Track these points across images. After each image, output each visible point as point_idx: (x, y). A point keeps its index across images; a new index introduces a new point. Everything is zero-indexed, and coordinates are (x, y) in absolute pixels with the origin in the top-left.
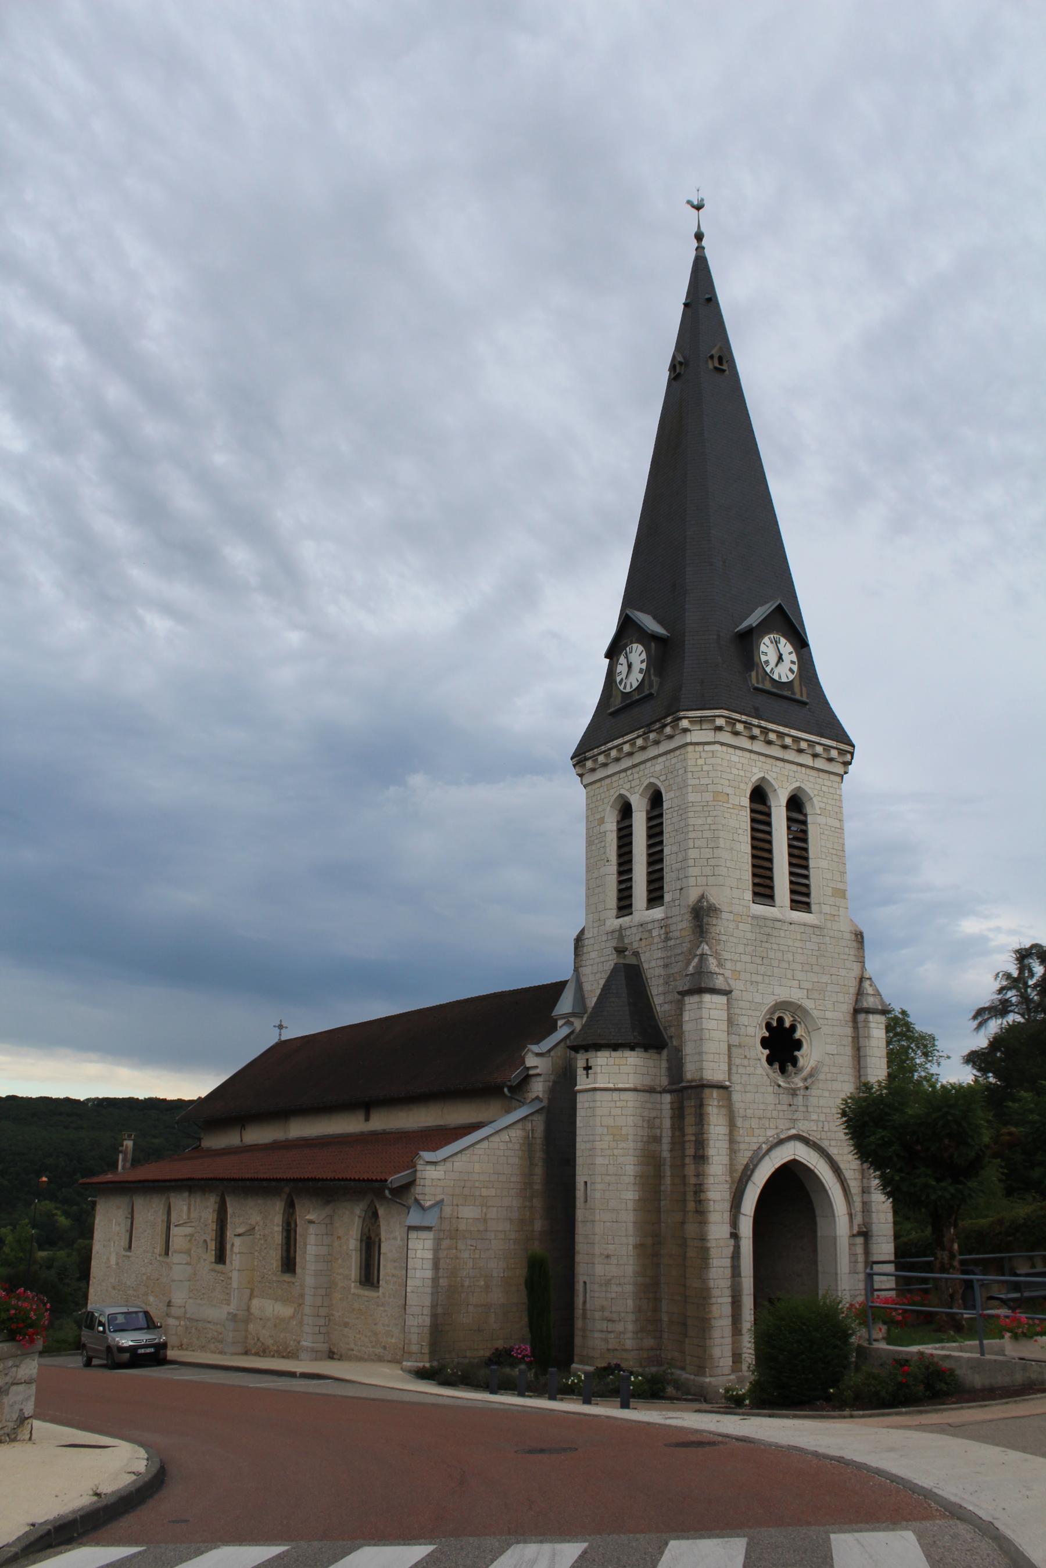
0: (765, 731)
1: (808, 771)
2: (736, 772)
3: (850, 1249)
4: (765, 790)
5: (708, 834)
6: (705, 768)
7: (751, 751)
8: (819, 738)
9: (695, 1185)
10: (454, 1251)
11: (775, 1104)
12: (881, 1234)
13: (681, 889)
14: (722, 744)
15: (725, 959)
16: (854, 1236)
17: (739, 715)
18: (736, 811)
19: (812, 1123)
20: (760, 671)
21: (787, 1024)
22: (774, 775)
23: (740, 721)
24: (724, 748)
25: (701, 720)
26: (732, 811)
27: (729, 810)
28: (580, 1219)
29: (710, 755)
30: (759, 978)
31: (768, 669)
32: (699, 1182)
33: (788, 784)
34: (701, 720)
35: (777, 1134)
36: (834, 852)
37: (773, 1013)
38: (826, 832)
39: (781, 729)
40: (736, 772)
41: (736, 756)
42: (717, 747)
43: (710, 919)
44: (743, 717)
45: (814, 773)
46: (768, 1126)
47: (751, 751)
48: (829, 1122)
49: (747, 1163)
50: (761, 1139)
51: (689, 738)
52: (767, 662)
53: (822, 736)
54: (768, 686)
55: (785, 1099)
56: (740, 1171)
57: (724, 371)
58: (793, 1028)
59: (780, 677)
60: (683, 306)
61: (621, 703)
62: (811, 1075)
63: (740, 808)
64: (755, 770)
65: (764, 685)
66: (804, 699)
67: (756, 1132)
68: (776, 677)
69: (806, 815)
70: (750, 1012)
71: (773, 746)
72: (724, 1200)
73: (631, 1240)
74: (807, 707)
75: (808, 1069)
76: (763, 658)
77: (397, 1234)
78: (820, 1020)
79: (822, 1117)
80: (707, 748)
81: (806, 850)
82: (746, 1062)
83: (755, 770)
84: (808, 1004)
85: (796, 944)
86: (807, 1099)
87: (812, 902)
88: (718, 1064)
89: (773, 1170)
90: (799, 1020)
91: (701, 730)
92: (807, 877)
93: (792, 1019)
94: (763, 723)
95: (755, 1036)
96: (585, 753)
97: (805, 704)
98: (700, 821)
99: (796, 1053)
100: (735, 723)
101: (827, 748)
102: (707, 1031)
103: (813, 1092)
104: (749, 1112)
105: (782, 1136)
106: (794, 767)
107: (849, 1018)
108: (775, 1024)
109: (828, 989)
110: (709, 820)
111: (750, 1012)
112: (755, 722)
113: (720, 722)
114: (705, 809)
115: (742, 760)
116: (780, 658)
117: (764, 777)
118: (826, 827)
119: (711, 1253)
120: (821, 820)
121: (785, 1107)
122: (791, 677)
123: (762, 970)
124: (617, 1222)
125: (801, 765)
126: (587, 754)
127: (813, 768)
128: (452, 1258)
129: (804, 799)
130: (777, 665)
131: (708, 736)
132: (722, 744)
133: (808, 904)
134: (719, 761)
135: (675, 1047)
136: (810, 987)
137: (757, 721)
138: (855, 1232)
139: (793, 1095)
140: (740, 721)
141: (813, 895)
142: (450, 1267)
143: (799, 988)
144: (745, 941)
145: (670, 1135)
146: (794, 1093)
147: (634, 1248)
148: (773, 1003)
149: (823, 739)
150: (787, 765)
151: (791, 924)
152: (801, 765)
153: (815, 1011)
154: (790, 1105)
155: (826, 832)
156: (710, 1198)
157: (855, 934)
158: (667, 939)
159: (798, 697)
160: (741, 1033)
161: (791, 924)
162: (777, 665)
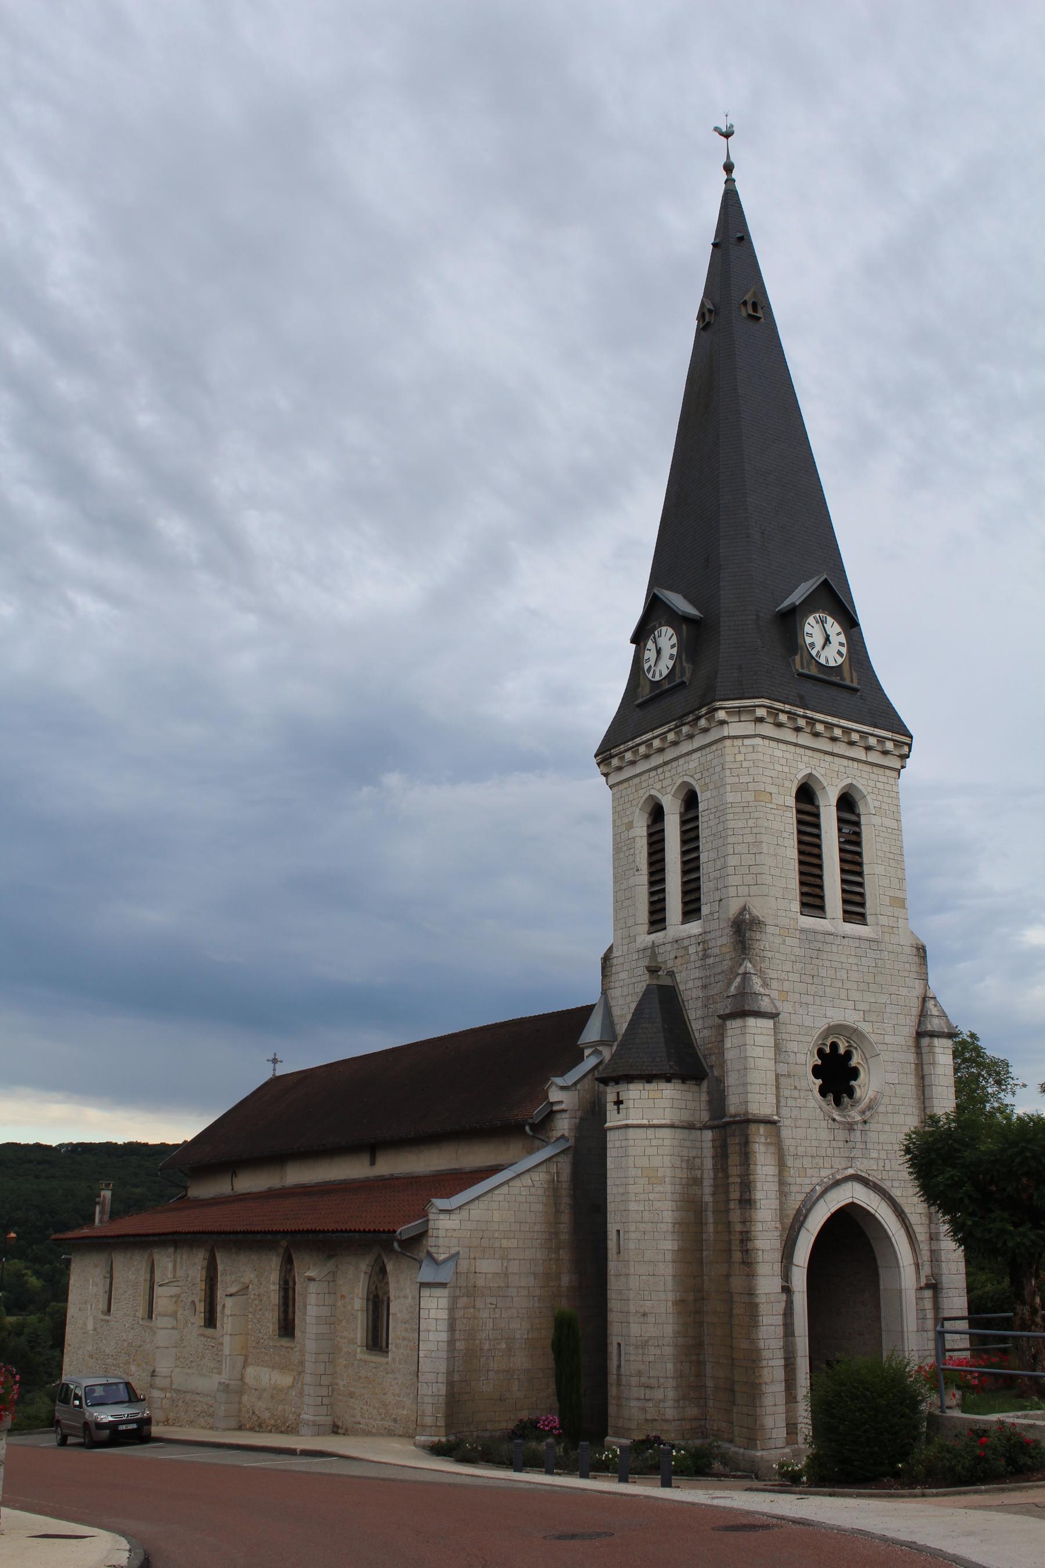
0: (811, 722)
3: (917, 1304)
5: (750, 839)
6: (745, 764)
7: (796, 745)
8: (873, 729)
9: (742, 1232)
10: (472, 1310)
11: (830, 1141)
12: (952, 1286)
13: (720, 900)
14: (764, 737)
15: (770, 978)
16: (921, 1288)
19: (872, 1161)
21: (842, 1050)
22: (823, 771)
23: (783, 711)
24: (766, 742)
25: (739, 711)
29: (751, 749)
30: (809, 999)
32: (745, 1230)
34: (739, 711)
35: (832, 1174)
36: (892, 856)
37: (826, 1038)
38: (882, 834)
39: (830, 719)
41: (779, 751)
43: (753, 934)
44: (786, 706)
46: (822, 1165)
47: (796, 745)
48: (890, 1160)
49: (800, 1207)
50: (815, 1180)
52: (812, 645)
54: (814, 671)
55: (842, 1134)
56: (792, 1217)
57: (759, 318)
58: (848, 1054)
59: (827, 661)
61: (650, 693)
62: (870, 1108)
63: (785, 809)
64: (801, 766)
65: (809, 670)
66: (855, 685)
67: (809, 1172)
69: (859, 815)
70: (800, 1038)
72: (774, 1249)
73: (671, 1296)
75: (867, 1100)
78: (878, 1045)
79: (883, 1155)
80: (747, 742)
81: (860, 854)
82: (796, 1094)
83: (801, 766)
84: (865, 1028)
85: (850, 961)
86: (866, 1134)
87: (868, 913)
88: (765, 1095)
89: (829, 1214)
90: (855, 1045)
91: (740, 721)
92: (861, 885)
93: (847, 1044)
94: (809, 713)
95: (806, 1064)
96: (610, 750)
97: (856, 690)
98: (740, 824)
99: (853, 1083)
100: (778, 714)
102: (752, 1059)
103: (873, 1126)
104: (801, 1150)
105: (838, 1177)
106: (845, 762)
107: (911, 1042)
108: (828, 1050)
109: (888, 1010)
110: (751, 823)
111: (800, 1038)
112: (800, 711)
113: (761, 712)
114: (746, 810)
115: (787, 755)
118: (881, 829)
119: (760, 1309)
120: (876, 820)
121: (841, 1144)
123: (812, 989)
124: (654, 1275)
125: (853, 759)
127: (866, 762)
128: (470, 1319)
129: (857, 797)
130: (823, 648)
131: (749, 728)
132: (764, 737)
133: (863, 915)
136: (867, 1008)
137: (802, 710)
138: (923, 1284)
139: (849, 1130)
140: (783, 711)
141: (868, 905)
142: (468, 1328)
143: (855, 1009)
144: (793, 958)
146: (850, 1127)
147: (673, 1305)
148: (826, 1026)
149: (876, 730)
150: (837, 760)
151: (844, 937)
152: (853, 759)
153: (873, 1035)
154: (847, 1142)
155: (882, 834)
156: (758, 1248)
157: (916, 948)
159: (848, 683)
160: (791, 1062)
161: (844, 937)
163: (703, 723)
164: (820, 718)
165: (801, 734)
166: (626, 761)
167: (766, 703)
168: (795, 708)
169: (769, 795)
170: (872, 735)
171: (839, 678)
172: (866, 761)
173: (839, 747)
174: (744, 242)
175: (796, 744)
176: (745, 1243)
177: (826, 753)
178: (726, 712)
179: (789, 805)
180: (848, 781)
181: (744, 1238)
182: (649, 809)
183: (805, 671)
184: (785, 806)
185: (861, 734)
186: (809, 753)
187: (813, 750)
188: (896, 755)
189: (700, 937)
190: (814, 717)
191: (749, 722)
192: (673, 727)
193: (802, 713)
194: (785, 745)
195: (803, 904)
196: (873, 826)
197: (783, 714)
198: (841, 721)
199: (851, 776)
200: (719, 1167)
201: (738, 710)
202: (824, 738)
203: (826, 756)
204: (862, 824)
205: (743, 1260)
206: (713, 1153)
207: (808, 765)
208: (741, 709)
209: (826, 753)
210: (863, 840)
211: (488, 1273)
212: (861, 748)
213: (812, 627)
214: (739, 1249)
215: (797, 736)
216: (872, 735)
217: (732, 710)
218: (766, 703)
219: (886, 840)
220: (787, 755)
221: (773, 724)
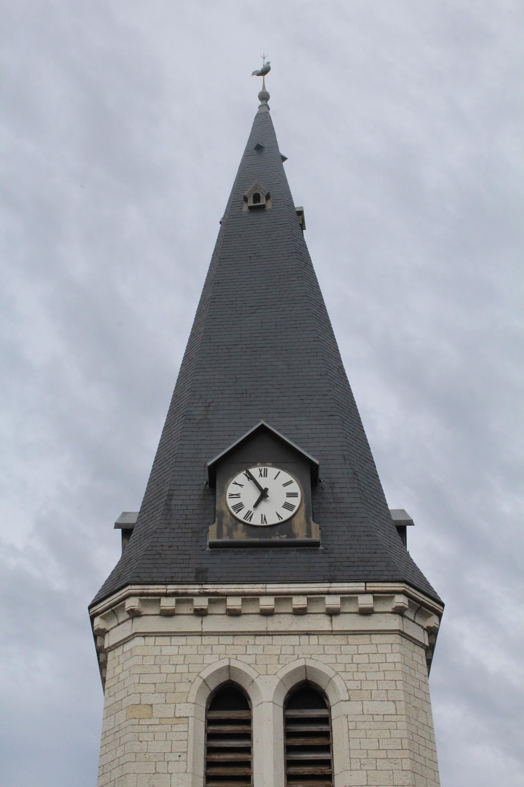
1: (323, 639)
2: (172, 669)
4: (316, 685)
7: (201, 634)
8: (328, 585)
14: (145, 635)
17: (163, 587)
18: (167, 728)
20: (227, 520)
22: (250, 659)
24: (150, 640)
26: (157, 728)
27: (151, 729)
29: (128, 655)
31: (241, 516)
33: (279, 666)
34: (113, 611)
36: (383, 754)
39: (247, 588)
40: (172, 669)
42: (138, 641)
44: (169, 587)
45: (339, 640)
47: (201, 634)
52: (239, 507)
53: (331, 581)
54: (240, 536)
57: (263, 207)
60: (283, 151)
63: (175, 721)
64: (208, 659)
66: (316, 537)
68: (256, 521)
71: (243, 618)
74: (321, 548)
76: (231, 503)
80: (127, 647)
83: (208, 659)
91: (119, 624)
94: (210, 588)
97: (316, 544)
100: (160, 600)
101: (378, 596)
106: (295, 640)
112: (195, 589)
113: (132, 603)
114: (118, 735)
116: (264, 494)
117: (229, 666)
118: (361, 718)
120: (346, 708)
122: (286, 514)
125: (308, 633)
127: (332, 633)
129: (322, 683)
132: (145, 635)
134: (137, 660)
140: (166, 595)
149: (334, 585)
150: (277, 639)
152: (308, 633)
155: (362, 726)
159: (301, 537)
162: (256, 506)
164: (229, 590)
165: (206, 619)
167: (137, 591)
168: (185, 587)
169: (148, 707)
170: (329, 593)
171: (285, 536)
172: (332, 631)
173: (280, 622)
175: (202, 632)
177: (257, 634)
178: (101, 617)
179: (182, 715)
180: (300, 663)
183: (225, 539)
184: (176, 718)
185: (309, 596)
186: (229, 640)
187: (234, 636)
188: (389, 612)
190: (219, 591)
191: (126, 622)
193: (197, 591)
194: (185, 638)
196: (344, 718)
197: (168, 598)
198: (268, 586)
199: (304, 656)
201: (110, 610)
202: (251, 616)
203: (258, 638)
204: (282, 708)
207: (222, 656)
208: (113, 608)
209: (257, 634)
210: (334, 741)
212: (320, 616)
213: (240, 485)
215: (202, 622)
216: (329, 593)
217: (106, 612)
218: (137, 591)
219: (369, 733)
220: (183, 650)
221: (160, 615)
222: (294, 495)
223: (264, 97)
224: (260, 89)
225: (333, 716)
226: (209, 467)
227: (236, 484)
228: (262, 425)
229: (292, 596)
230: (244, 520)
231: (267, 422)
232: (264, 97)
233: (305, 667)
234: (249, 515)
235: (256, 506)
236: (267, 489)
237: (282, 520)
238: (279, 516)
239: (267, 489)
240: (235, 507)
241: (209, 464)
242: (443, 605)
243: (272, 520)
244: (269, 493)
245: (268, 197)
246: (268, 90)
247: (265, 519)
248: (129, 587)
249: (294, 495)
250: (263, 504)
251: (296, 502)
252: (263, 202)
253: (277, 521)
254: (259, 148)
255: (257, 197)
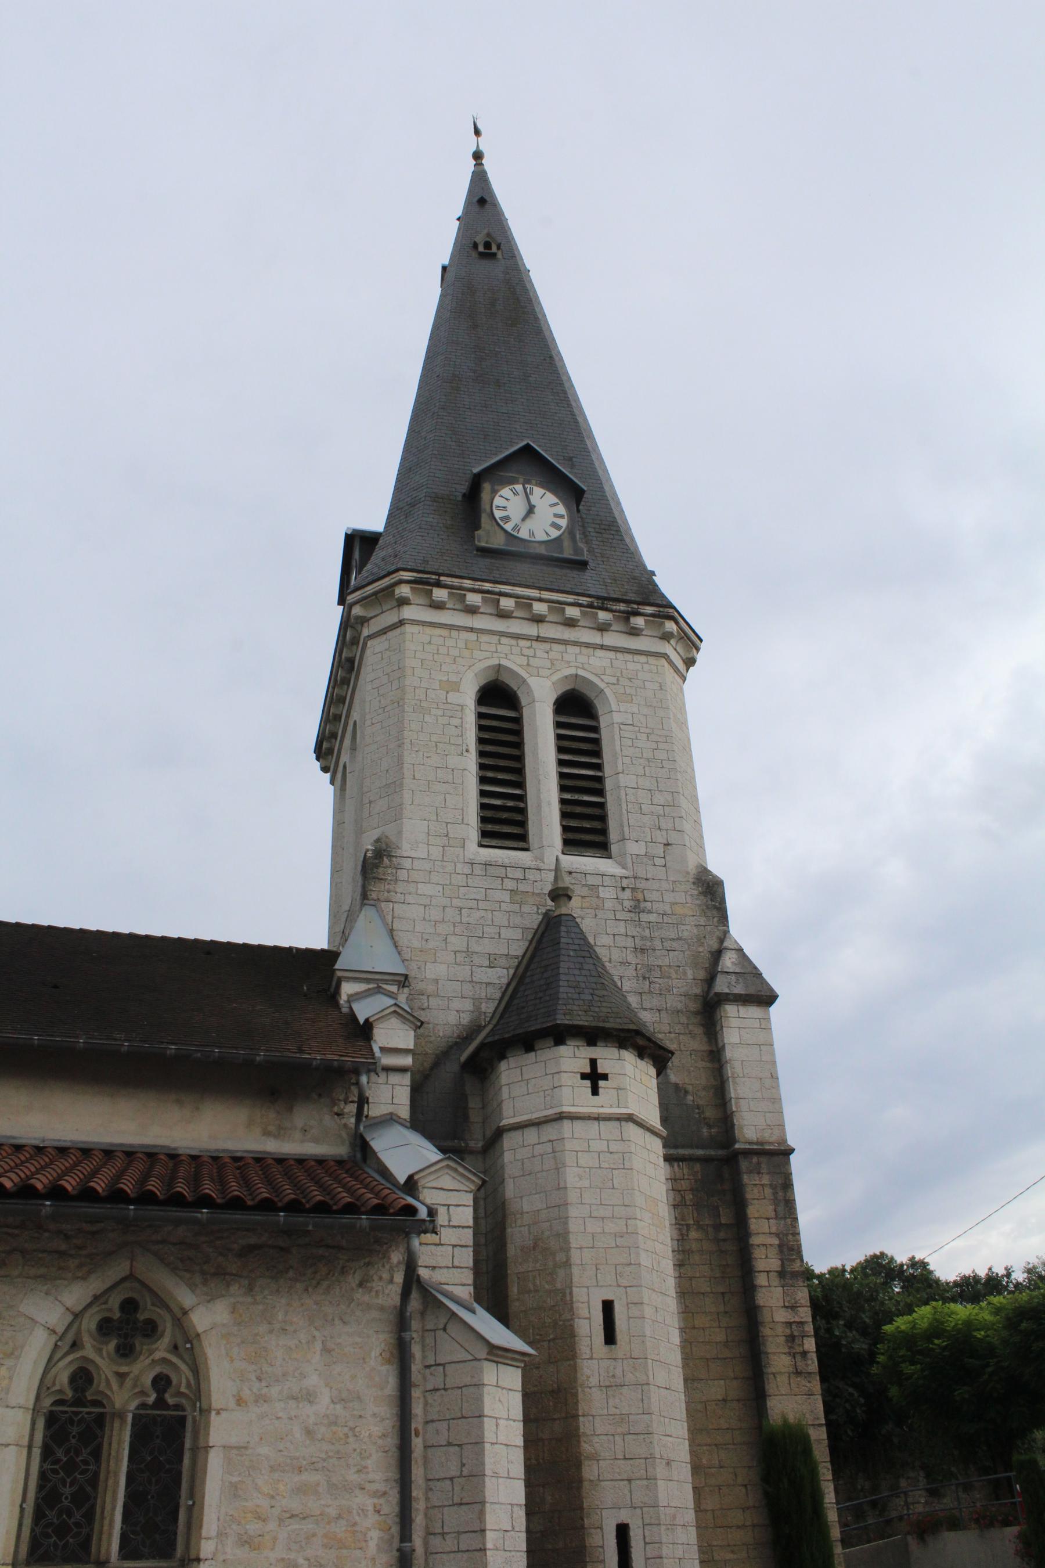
9: (789, 1324)
13: (667, 845)
28: (594, 1381)
31: (509, 527)
32: (797, 1319)
51: (408, 612)
57: (494, 255)
60: (650, 568)
61: (503, 545)
77: (313, 1380)
96: (440, 575)
116: (531, 510)
122: (555, 534)
126: (442, 578)
129: (591, 694)
135: (676, 1085)
145: (571, 1236)
158: (637, 908)
162: (524, 519)
163: (639, 622)
166: (396, 597)
172: (602, 645)
174: (487, 206)
176: (798, 1341)
181: (796, 1333)
182: (483, 682)
189: (624, 880)
190: (491, 585)
192: (585, 603)
195: (484, 834)
200: (692, 1222)
205: (797, 1369)
206: (674, 1199)
211: (771, 1271)
213: (507, 499)
214: (787, 1350)
222: (561, 516)
223: (478, 156)
224: (474, 149)
225: (602, 726)
226: (475, 475)
227: (502, 497)
228: (528, 444)
229: (566, 606)
230: (512, 532)
231: (531, 441)
232: (478, 156)
233: (576, 675)
234: (516, 527)
235: (524, 519)
236: (534, 506)
237: (550, 538)
238: (547, 533)
239: (534, 506)
240: (502, 518)
241: (476, 470)
242: (701, 640)
243: (541, 537)
244: (536, 510)
245: (499, 247)
246: (481, 148)
247: (533, 533)
248: (402, 573)
249: (561, 516)
250: (528, 521)
251: (563, 523)
252: (494, 249)
253: (545, 538)
254: (482, 202)
255: (487, 245)
